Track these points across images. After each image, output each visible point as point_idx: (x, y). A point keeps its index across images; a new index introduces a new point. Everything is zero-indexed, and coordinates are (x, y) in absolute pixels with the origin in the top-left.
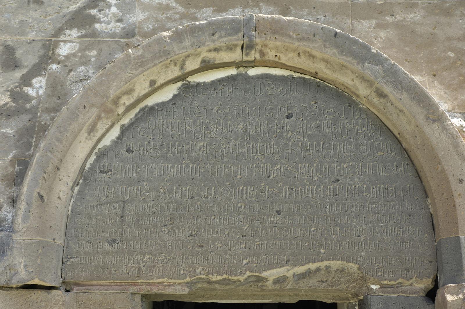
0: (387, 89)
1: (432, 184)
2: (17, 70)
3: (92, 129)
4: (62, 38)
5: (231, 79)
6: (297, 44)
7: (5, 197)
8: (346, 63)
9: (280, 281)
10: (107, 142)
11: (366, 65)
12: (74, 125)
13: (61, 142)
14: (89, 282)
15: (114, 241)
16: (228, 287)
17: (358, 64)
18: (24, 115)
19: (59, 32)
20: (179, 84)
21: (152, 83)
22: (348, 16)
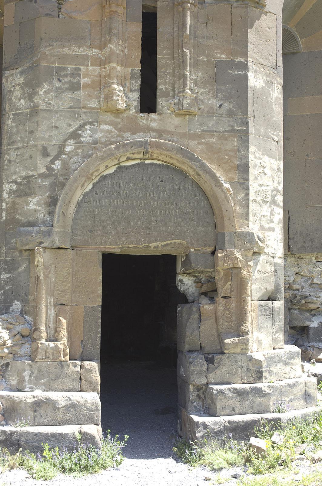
0: (201, 173)
1: (216, 211)
2: (48, 157)
3: (83, 186)
4: (67, 144)
5: (138, 164)
6: (166, 152)
7: (46, 211)
8: (185, 161)
9: (156, 247)
10: (87, 190)
11: (193, 162)
12: (76, 184)
13: (71, 191)
14: (81, 247)
15: (91, 231)
16: (136, 249)
17: (190, 162)
18: (52, 177)
19: (65, 141)
20: (117, 166)
21: (107, 166)
22: (186, 139)
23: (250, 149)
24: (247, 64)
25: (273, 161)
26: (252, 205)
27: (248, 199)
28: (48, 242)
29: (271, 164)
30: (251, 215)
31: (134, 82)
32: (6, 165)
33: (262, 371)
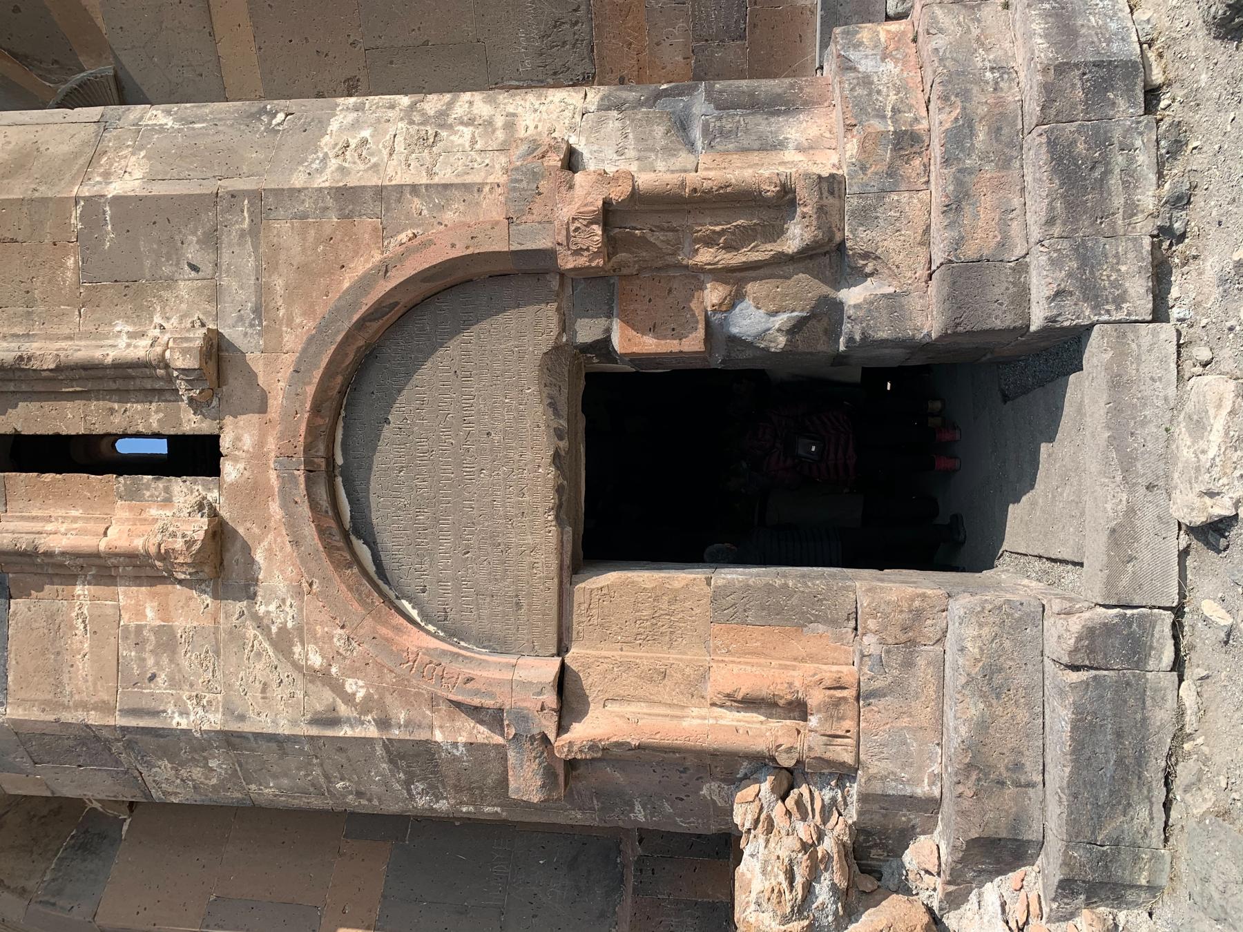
19: (296, 666)
20: (353, 538)
23: (298, 186)
24: (86, 199)
25: (334, 125)
26: (445, 175)
27: (427, 186)
28: (544, 722)
29: (341, 129)
30: (468, 179)
31: (148, 494)
32: (370, 800)
33: (895, 132)
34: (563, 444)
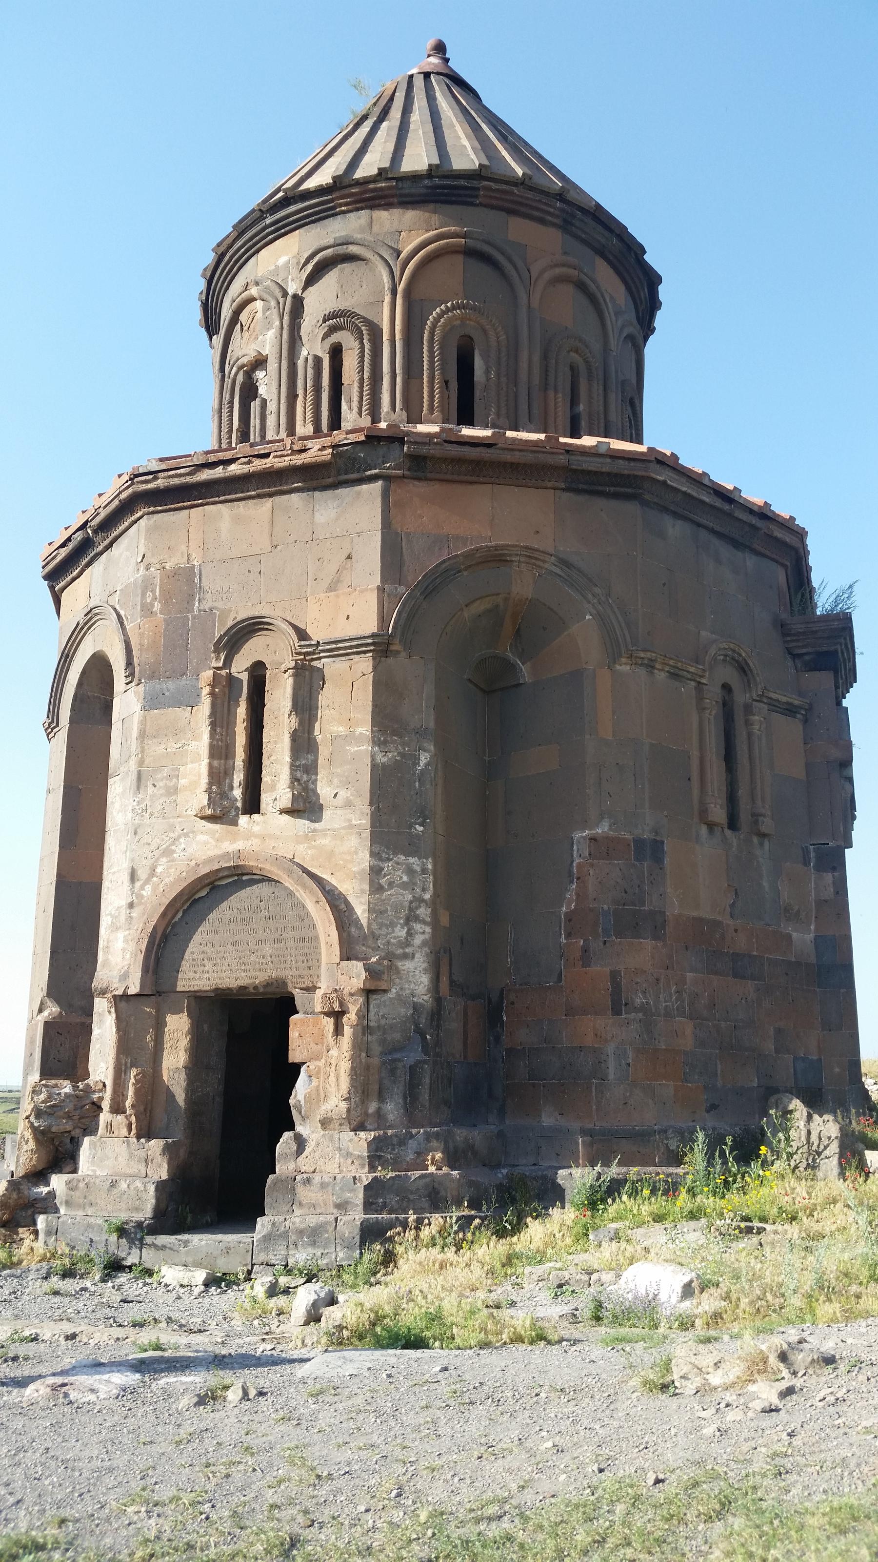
34: (252, 990)
